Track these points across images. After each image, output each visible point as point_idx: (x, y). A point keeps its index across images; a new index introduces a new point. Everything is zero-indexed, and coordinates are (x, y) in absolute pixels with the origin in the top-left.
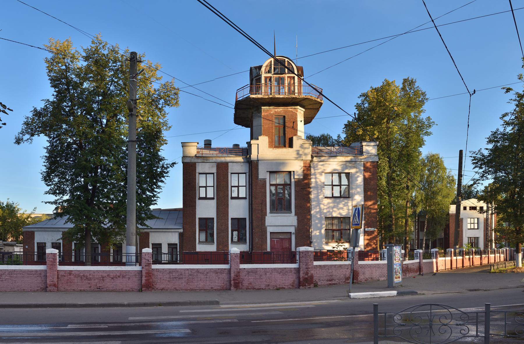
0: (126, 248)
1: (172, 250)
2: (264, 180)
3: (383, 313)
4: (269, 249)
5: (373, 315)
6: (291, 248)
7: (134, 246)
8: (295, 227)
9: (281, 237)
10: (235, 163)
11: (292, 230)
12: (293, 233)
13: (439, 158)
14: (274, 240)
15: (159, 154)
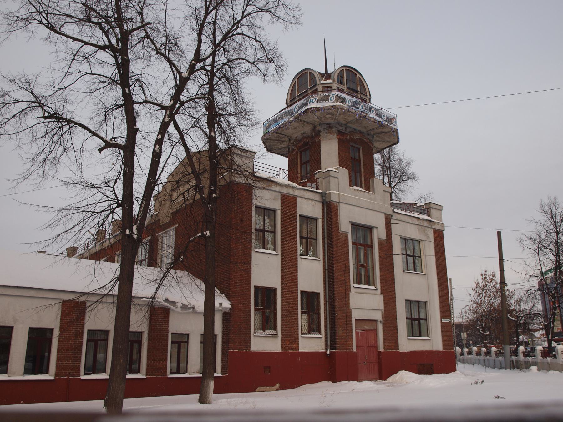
0: (383, 213)
1: (142, 20)
6: (376, 347)
7: (539, 362)
8: (382, 312)
9: (366, 327)
10: (305, 200)
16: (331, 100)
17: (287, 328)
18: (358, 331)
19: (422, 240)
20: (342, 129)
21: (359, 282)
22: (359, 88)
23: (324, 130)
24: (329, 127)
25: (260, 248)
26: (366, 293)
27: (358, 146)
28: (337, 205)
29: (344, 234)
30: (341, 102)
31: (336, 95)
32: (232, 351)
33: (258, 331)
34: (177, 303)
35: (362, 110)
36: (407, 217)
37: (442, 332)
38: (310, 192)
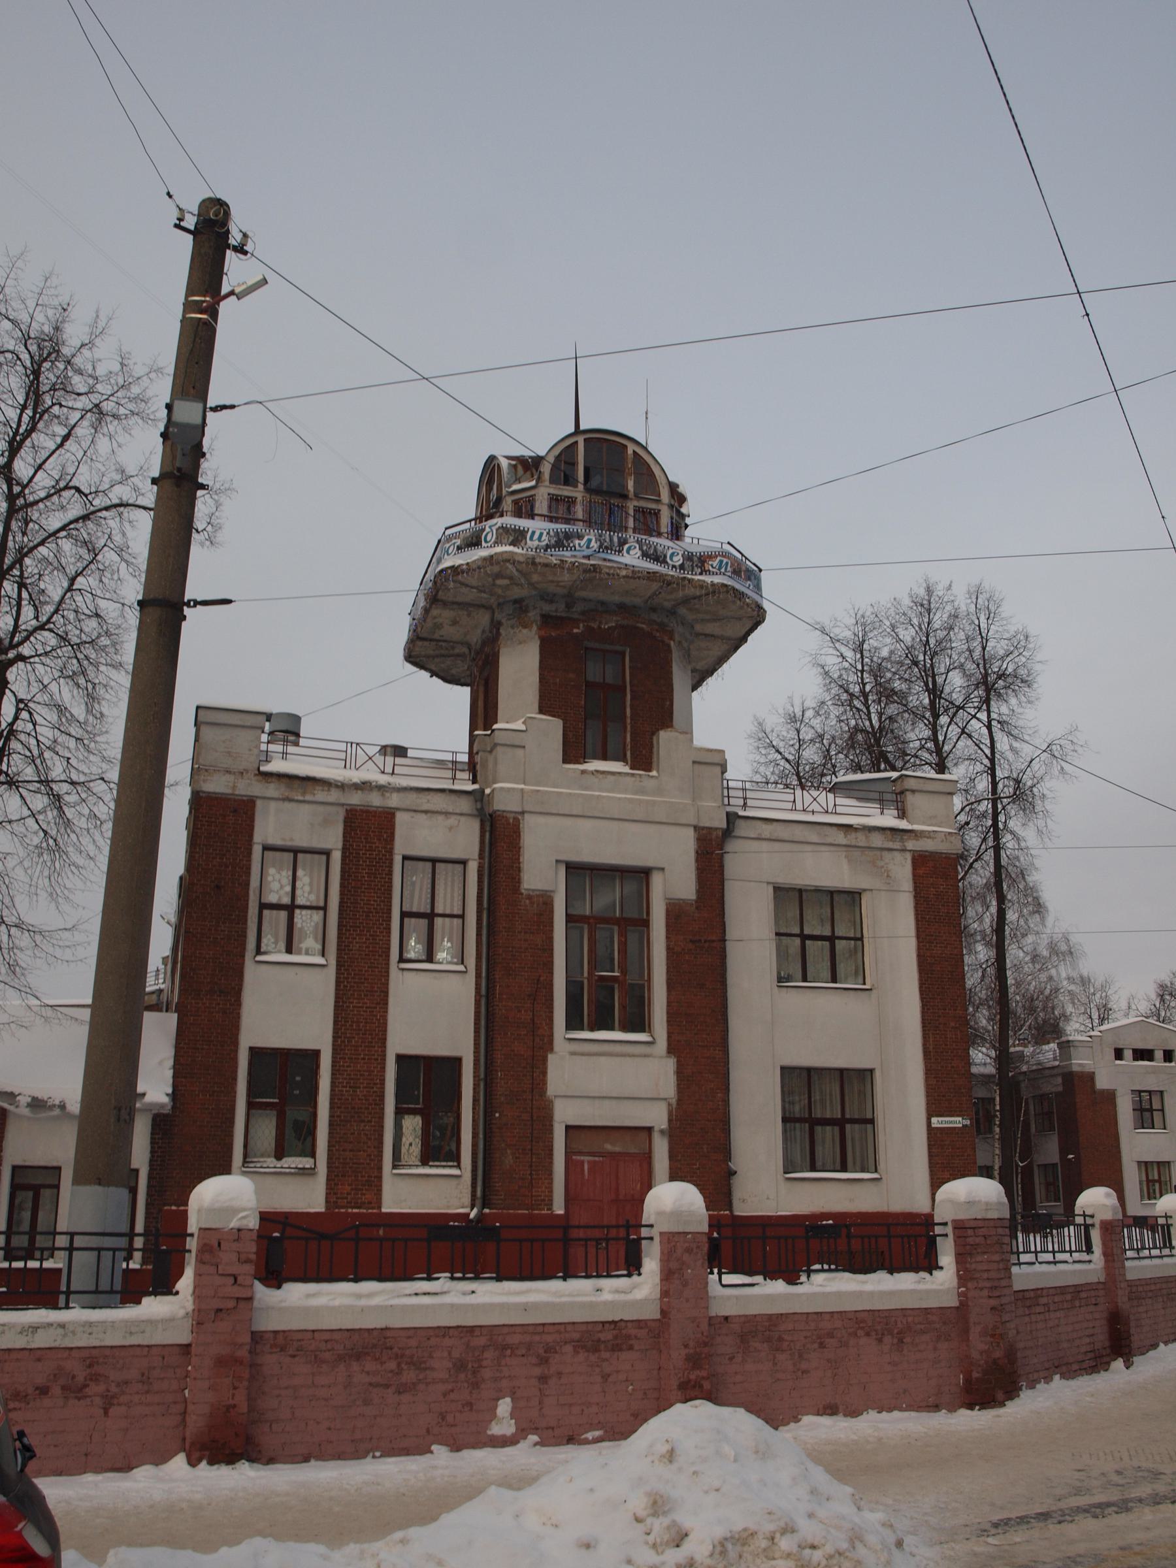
2: (545, 902)
3: (1160, 1177)
4: (559, 1210)
5: (618, 915)
8: (669, 1105)
9: (609, 1147)
11: (657, 1117)
12: (662, 1132)
13: (1015, 1372)
14: (582, 1162)
15: (971, 1053)
16: (486, 541)
17: (344, 1150)
18: (582, 1158)
19: (865, 890)
20: (559, 609)
21: (574, 1022)
22: (631, 485)
23: (509, 619)
24: (520, 607)
25: (280, 952)
26: (583, 1054)
27: (618, 648)
28: (519, 820)
29: (538, 896)
30: (513, 544)
31: (499, 525)
32: (174, 1208)
33: (262, 1160)
34: (19, 1094)
35: (587, 552)
36: (801, 827)
37: (931, 1156)
38: (440, 794)
